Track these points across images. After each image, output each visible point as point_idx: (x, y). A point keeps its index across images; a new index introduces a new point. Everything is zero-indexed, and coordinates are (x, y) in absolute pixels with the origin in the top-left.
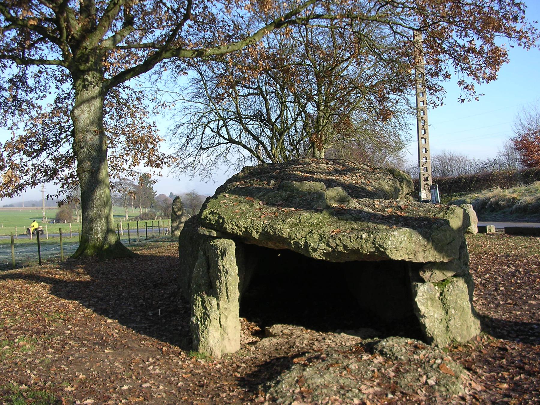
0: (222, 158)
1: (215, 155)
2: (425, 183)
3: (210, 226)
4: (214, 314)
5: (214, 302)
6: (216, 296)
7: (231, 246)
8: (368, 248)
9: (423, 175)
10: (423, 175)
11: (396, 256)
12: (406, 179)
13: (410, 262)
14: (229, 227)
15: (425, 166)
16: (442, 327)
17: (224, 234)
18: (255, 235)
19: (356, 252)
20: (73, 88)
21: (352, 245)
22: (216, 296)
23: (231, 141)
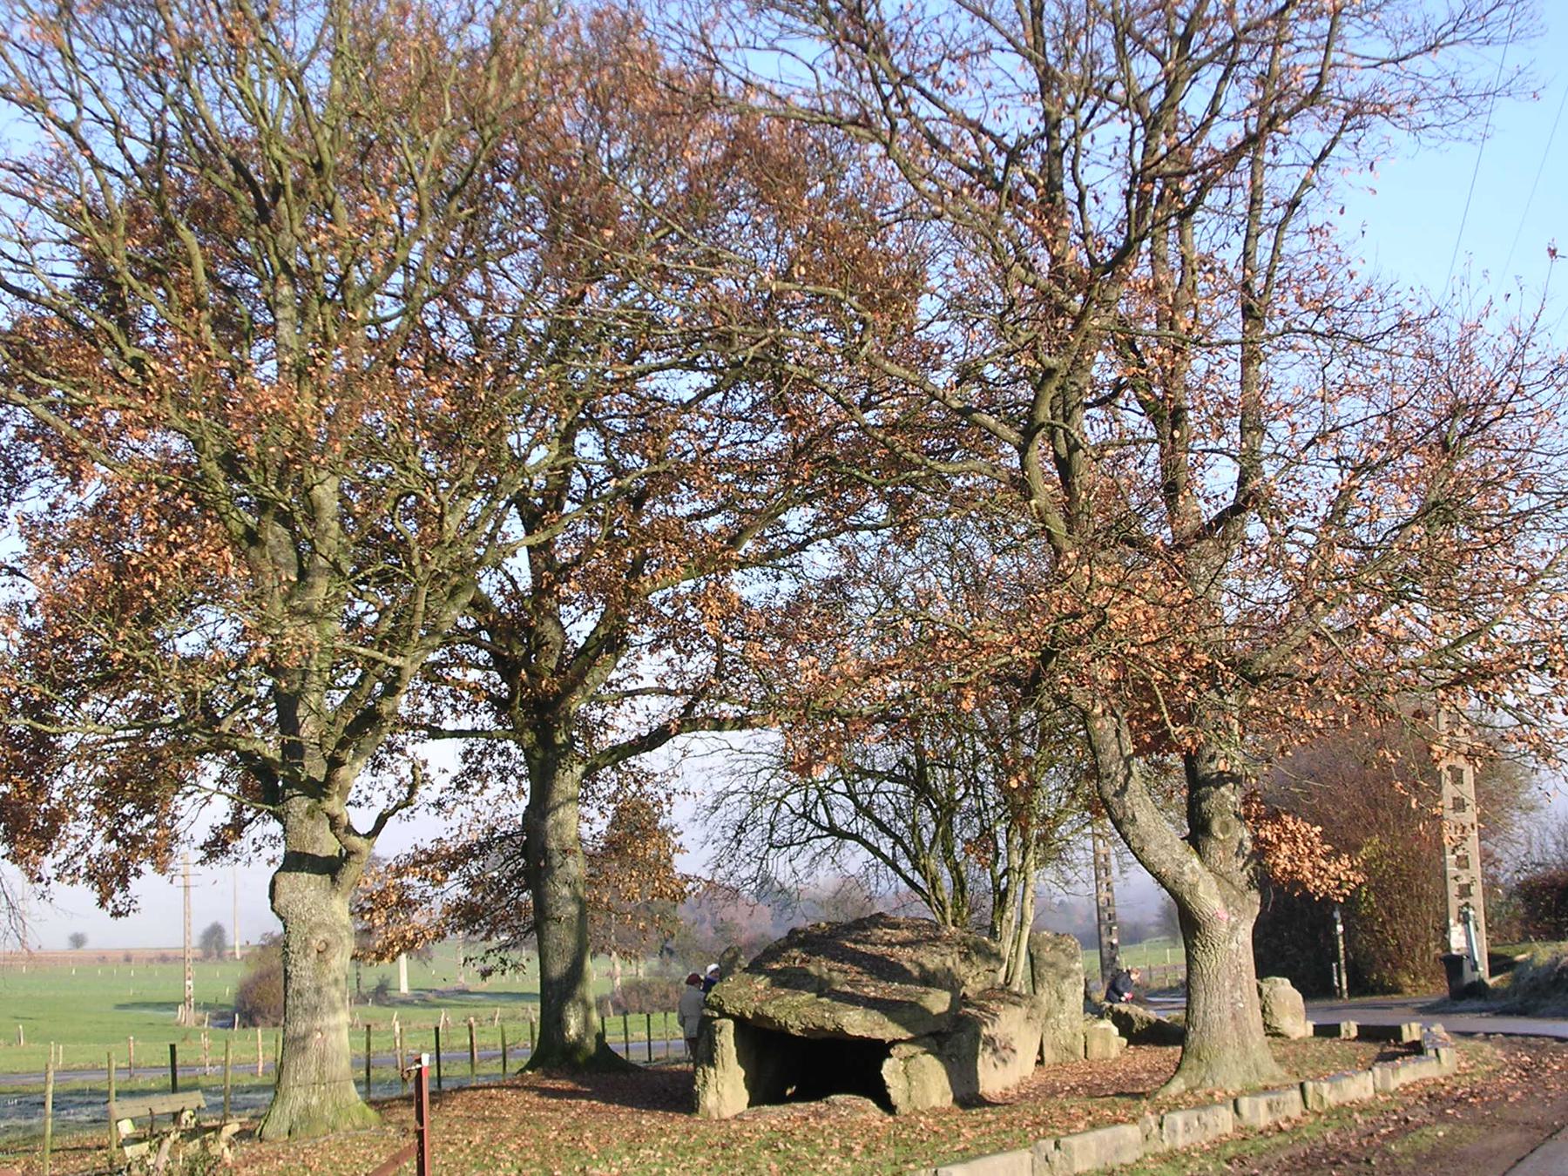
0: (827, 861)
1: (808, 857)
2: (1462, 902)
3: (713, 1008)
4: (712, 1081)
5: (712, 1071)
6: (714, 1066)
7: (729, 1026)
8: (830, 1026)
9: (1456, 878)
10: (1456, 878)
11: (854, 1032)
12: (295, 1044)
13: (869, 1039)
14: (727, 1008)
15: (1459, 853)
16: (905, 1097)
17: (724, 1015)
18: (749, 1016)
19: (822, 1029)
20: (591, 858)
21: (818, 1022)
22: (714, 1066)
23: (833, 830)
